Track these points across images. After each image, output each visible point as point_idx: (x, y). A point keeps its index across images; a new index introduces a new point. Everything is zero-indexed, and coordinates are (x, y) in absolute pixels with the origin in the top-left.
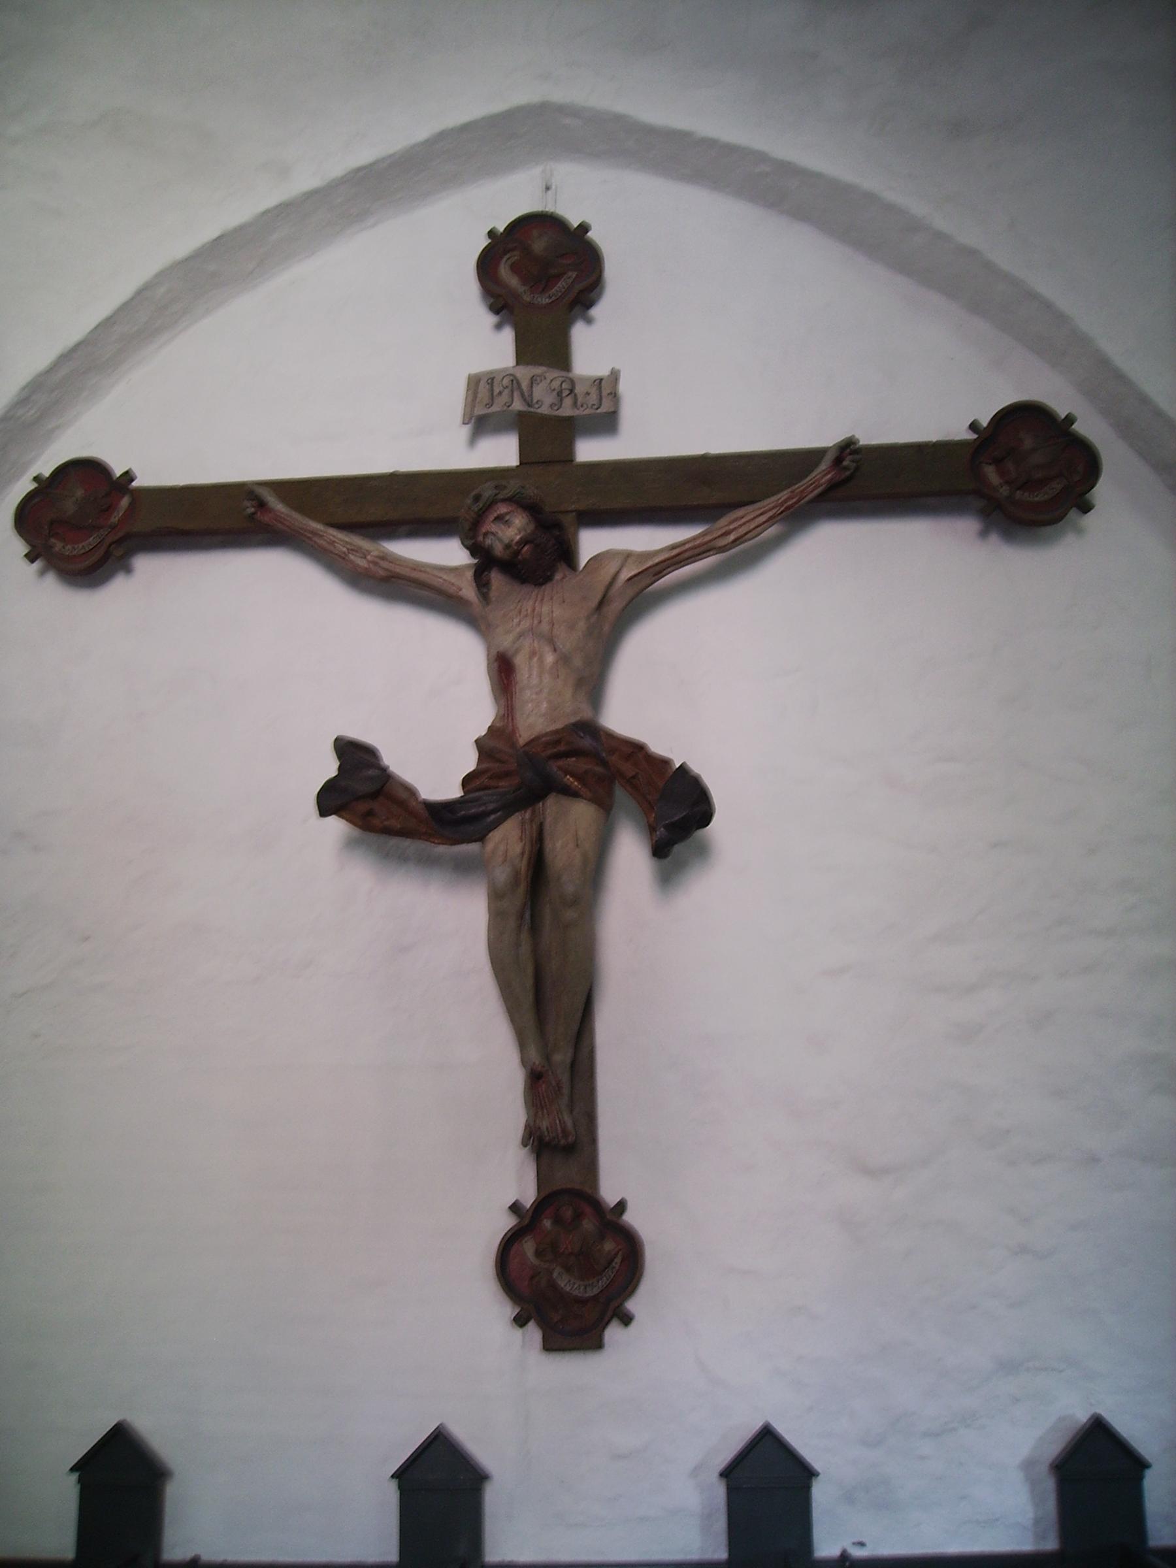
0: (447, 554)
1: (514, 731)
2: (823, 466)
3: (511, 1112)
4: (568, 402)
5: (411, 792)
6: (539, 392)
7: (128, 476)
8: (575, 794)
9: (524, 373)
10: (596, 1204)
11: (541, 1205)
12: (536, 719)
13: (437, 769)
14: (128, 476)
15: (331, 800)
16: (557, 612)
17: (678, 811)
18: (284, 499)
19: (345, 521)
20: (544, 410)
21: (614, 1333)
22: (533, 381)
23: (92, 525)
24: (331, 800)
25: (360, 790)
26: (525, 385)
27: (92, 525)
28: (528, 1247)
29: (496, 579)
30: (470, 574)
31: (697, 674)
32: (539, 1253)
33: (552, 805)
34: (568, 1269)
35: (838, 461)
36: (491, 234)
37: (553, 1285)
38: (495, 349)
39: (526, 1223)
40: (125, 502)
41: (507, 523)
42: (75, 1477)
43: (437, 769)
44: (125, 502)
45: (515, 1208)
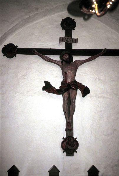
0: (57, 58)
1: (67, 81)
2: (102, 51)
3: (64, 127)
4: (72, 41)
5: (55, 88)
6: (68, 40)
7: (17, 46)
8: (74, 89)
9: (66, 37)
10: (73, 138)
11: (66, 138)
12: (69, 80)
13: (57, 84)
14: (17, 46)
15: (44, 89)
16: (72, 67)
17: (86, 91)
18: (37, 51)
19: (44, 53)
20: (69, 42)
21: (75, 153)
22: (68, 38)
23: (11, 51)
24: (44, 89)
25: (48, 87)
26: (67, 39)
27: (11, 51)
28: (65, 143)
29: (64, 62)
30: (61, 62)
31: (85, 75)
32: (66, 144)
33: (71, 90)
34: (70, 146)
35: (104, 51)
36: (63, 19)
37: (68, 148)
38: (63, 34)
39: (65, 140)
40: (16, 49)
41: (66, 56)
42: (8, 172)
43: (57, 84)
44: (16, 49)
45: (63, 138)
